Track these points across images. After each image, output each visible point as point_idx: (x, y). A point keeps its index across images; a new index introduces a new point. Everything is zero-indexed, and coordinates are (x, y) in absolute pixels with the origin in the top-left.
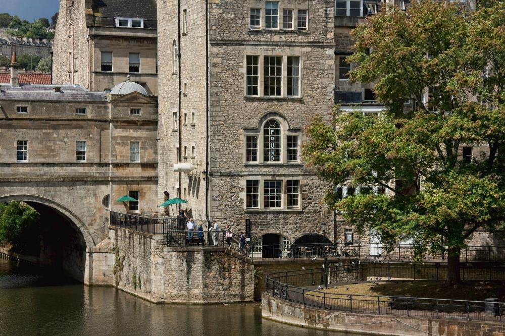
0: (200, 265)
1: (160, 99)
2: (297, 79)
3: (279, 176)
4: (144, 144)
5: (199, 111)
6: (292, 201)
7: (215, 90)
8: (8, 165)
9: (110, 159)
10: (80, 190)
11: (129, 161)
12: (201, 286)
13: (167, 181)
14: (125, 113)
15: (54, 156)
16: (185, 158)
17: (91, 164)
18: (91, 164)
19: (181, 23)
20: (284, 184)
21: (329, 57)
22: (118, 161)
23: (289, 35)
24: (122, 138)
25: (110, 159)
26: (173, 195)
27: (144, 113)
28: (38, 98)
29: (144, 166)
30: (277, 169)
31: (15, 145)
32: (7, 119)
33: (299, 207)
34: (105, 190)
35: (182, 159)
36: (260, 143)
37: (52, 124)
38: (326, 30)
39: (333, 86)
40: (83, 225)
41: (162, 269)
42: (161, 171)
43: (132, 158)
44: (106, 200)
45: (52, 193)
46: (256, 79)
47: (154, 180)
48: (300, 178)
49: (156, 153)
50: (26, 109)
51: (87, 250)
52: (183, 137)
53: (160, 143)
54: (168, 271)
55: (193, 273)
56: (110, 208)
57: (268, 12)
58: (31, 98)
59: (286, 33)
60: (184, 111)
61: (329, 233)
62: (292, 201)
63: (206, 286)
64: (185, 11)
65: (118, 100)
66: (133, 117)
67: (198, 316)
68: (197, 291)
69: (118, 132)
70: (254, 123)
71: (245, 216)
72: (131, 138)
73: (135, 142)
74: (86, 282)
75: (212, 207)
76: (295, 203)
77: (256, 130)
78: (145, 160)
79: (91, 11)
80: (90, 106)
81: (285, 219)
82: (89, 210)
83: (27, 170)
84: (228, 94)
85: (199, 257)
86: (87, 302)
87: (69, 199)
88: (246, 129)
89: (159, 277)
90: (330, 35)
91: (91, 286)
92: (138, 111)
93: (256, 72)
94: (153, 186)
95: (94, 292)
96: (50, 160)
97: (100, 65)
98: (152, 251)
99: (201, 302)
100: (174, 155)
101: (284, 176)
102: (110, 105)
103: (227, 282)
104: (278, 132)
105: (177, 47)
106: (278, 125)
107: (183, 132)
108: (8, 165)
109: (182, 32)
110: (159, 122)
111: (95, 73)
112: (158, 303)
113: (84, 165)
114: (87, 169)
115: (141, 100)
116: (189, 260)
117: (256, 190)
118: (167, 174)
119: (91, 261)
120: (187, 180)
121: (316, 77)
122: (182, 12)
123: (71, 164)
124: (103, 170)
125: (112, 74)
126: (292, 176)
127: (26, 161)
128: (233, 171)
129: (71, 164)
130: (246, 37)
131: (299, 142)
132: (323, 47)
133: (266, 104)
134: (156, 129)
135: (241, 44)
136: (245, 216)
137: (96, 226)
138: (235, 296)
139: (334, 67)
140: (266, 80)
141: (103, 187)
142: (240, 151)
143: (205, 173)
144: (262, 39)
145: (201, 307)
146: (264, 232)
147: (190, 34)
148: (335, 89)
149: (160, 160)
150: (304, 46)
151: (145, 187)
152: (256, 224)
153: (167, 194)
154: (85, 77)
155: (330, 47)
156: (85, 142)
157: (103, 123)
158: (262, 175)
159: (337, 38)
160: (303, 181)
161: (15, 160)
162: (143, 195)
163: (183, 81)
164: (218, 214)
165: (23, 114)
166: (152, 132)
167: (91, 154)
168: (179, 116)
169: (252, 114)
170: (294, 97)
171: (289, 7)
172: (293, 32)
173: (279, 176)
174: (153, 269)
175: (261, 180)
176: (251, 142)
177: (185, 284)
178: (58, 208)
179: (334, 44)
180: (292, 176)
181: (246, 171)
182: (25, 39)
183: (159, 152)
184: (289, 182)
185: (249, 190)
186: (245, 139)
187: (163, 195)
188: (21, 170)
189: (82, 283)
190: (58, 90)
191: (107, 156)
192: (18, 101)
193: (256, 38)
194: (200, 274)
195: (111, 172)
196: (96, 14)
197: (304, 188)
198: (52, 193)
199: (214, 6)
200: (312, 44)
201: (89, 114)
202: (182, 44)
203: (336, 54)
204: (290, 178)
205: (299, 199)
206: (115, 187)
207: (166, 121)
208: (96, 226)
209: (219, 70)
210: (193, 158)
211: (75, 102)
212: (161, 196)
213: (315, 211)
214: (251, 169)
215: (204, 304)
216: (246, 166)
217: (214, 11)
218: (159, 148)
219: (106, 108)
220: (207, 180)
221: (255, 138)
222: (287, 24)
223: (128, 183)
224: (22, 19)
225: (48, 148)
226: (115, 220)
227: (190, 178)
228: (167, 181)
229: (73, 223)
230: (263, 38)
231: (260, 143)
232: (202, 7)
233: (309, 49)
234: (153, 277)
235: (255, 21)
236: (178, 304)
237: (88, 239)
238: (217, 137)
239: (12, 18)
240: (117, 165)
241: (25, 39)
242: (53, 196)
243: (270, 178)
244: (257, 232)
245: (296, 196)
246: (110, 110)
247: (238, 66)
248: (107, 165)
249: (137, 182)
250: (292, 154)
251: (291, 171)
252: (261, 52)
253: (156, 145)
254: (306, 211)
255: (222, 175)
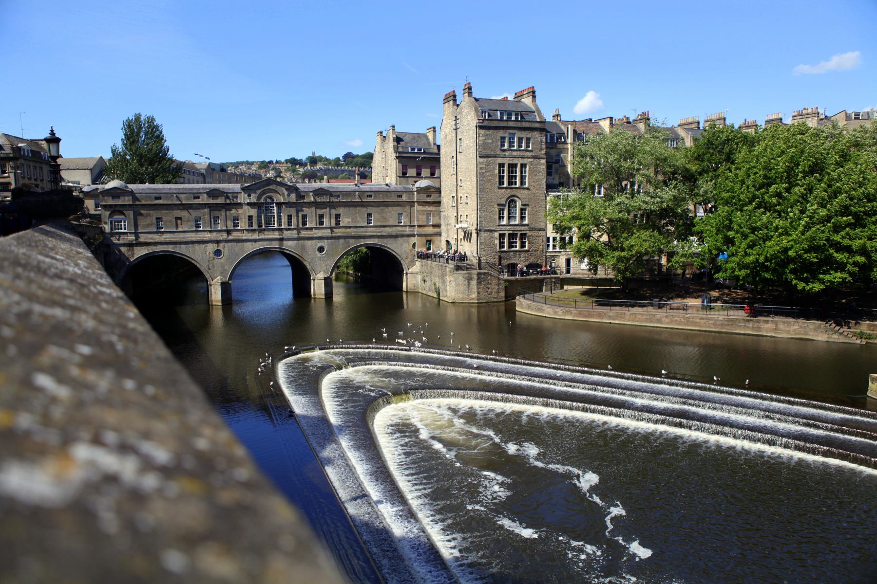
0: (476, 281)
1: (443, 190)
2: (526, 176)
3: (516, 231)
4: (434, 214)
5: (471, 194)
6: (523, 246)
7: (482, 183)
8: (362, 227)
9: (416, 222)
10: (400, 240)
11: (426, 224)
12: (476, 293)
13: (448, 234)
14: (424, 198)
15: (386, 222)
16: (461, 222)
17: (406, 226)
18: (406, 226)
19: (458, 146)
20: (519, 235)
21: (543, 164)
22: (420, 224)
23: (521, 152)
24: (422, 211)
25: (416, 222)
26: (453, 242)
27: (433, 198)
28: (377, 190)
29: (434, 226)
30: (515, 227)
31: (366, 216)
32: (362, 202)
33: (526, 248)
34: (414, 240)
35: (459, 222)
36: (506, 212)
37: (386, 204)
38: (541, 149)
39: (545, 180)
40: (402, 259)
41: (453, 284)
42: (443, 229)
43: (428, 222)
44: (414, 245)
45: (386, 242)
46: (503, 177)
47: (440, 235)
48: (527, 232)
49: (440, 219)
50: (371, 196)
51: (405, 272)
52: (459, 210)
53: (442, 214)
54: (457, 284)
55: (471, 286)
56: (416, 250)
57: (510, 139)
58: (374, 190)
59: (520, 150)
60: (459, 195)
61: (542, 262)
62: (523, 246)
63: (479, 293)
64: (460, 139)
65: (420, 190)
66: (429, 200)
67: (474, 311)
68: (474, 296)
69: (421, 208)
70: (503, 201)
71: (499, 254)
72: (426, 211)
73: (429, 214)
74: (313, 296)
75: (480, 249)
76: (525, 246)
77: (504, 205)
78: (435, 223)
79: (396, 143)
80: (405, 194)
81: (519, 255)
82: (405, 251)
83: (372, 229)
84: (489, 185)
85: (475, 277)
86: (405, 301)
87: (395, 245)
88: (499, 205)
89: (452, 288)
90: (543, 152)
91: (407, 292)
92: (430, 196)
93: (503, 173)
94: (439, 238)
95: (409, 296)
96: (384, 224)
97: (401, 172)
98: (448, 273)
99: (476, 302)
100: (452, 221)
101: (519, 231)
102: (415, 193)
103: (490, 290)
104: (515, 206)
105: (455, 160)
106: (515, 202)
107: (459, 207)
108: (362, 227)
109: (458, 151)
110: (442, 202)
111: (399, 177)
112: (451, 303)
113: (402, 226)
114: (404, 228)
115: (432, 190)
116: (469, 279)
117: (504, 239)
118: (448, 230)
119: (407, 279)
120: (463, 234)
121: (536, 175)
122: (458, 140)
123: (395, 226)
124: (412, 229)
125: (408, 177)
126: (523, 231)
127: (372, 225)
128: (492, 229)
129: (395, 226)
130: (498, 153)
131: (527, 212)
132: (539, 158)
133: (509, 191)
134: (440, 206)
135: (495, 157)
136: (499, 254)
137: (409, 260)
138: (494, 298)
139: (545, 170)
140: (509, 177)
141: (412, 238)
142: (495, 217)
143: (477, 229)
144: (507, 154)
145: (476, 305)
146: (508, 262)
147: (464, 152)
148: (546, 182)
149: (442, 223)
150: (530, 158)
151: (434, 238)
152: (504, 258)
153: (448, 242)
154: (393, 179)
155: (543, 158)
156: (402, 214)
157: (412, 204)
158: (507, 230)
159: (546, 153)
160: (529, 233)
161: (366, 224)
162: (434, 242)
163: (459, 179)
164: (483, 253)
165: (370, 199)
166: (437, 208)
167: (406, 220)
168: (456, 199)
169: (503, 195)
170: (525, 186)
171: (521, 136)
172: (523, 150)
173: (516, 231)
174: (448, 283)
175: (507, 233)
176: (501, 211)
177: (467, 292)
178: (389, 250)
179: (545, 157)
180: (523, 231)
181: (498, 228)
182: (330, 167)
183: (442, 218)
184: (521, 234)
185: (500, 239)
186: (498, 210)
187: (445, 242)
188: (369, 229)
189: (311, 296)
190: (387, 185)
191: (414, 221)
192: (367, 192)
193: (504, 153)
194: (476, 286)
195: (416, 230)
196: (399, 145)
197: (530, 238)
198: (386, 242)
199: (481, 135)
200: (534, 157)
201: (405, 198)
202: (458, 158)
203: (546, 162)
204: (522, 232)
205: (527, 244)
206: (419, 238)
207: (446, 198)
208: (409, 260)
209: (484, 171)
210: (466, 221)
211: (397, 192)
212: (444, 244)
213: (535, 250)
214: (501, 227)
215: (478, 303)
216: (499, 226)
217: (481, 138)
218: (442, 216)
219: (414, 194)
220: (477, 233)
221: (503, 210)
222: (520, 146)
223: (426, 235)
224: (328, 158)
225: (383, 217)
226: (421, 256)
227: (465, 233)
228: (448, 234)
229: (397, 258)
230: (507, 153)
231: (506, 212)
232: (473, 137)
233: (532, 160)
234: (448, 288)
235: (503, 145)
236: (463, 303)
237: (405, 266)
238: (483, 209)
239: (323, 158)
240: (419, 226)
241: (330, 167)
242: (386, 244)
243: (511, 232)
244: (505, 262)
245: (525, 242)
246: (415, 196)
247: (494, 169)
248: (414, 226)
249: (431, 235)
250: (522, 218)
251: (522, 228)
252: (507, 161)
253: (440, 214)
254: (531, 250)
255: (485, 231)
